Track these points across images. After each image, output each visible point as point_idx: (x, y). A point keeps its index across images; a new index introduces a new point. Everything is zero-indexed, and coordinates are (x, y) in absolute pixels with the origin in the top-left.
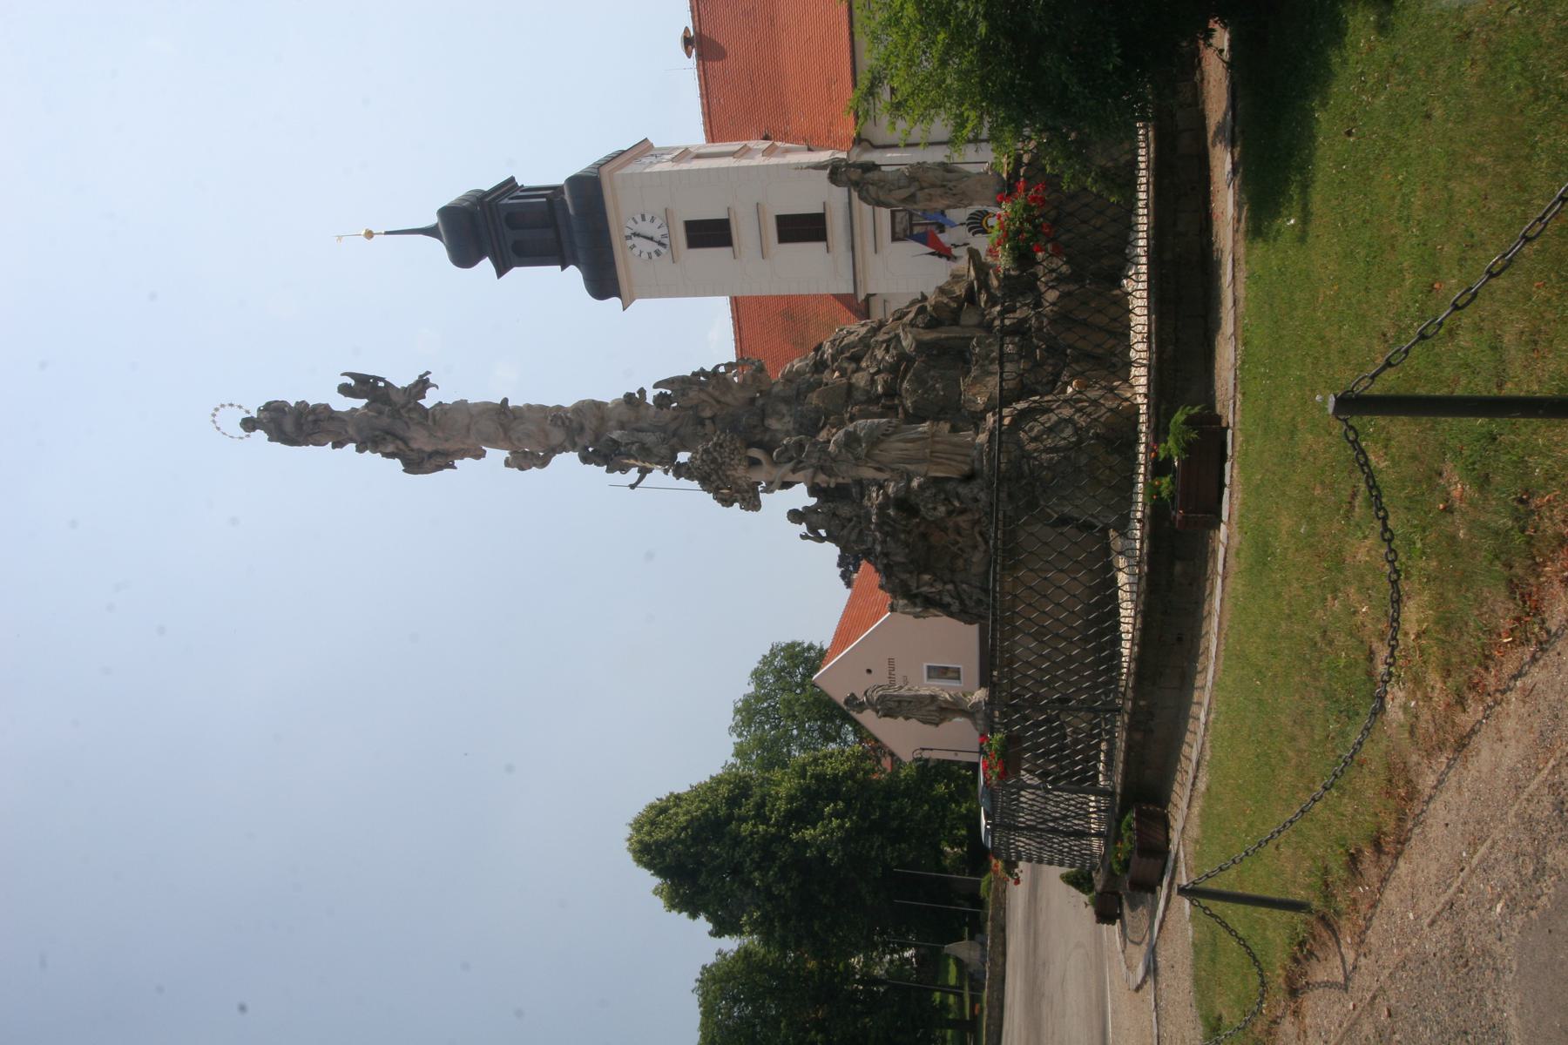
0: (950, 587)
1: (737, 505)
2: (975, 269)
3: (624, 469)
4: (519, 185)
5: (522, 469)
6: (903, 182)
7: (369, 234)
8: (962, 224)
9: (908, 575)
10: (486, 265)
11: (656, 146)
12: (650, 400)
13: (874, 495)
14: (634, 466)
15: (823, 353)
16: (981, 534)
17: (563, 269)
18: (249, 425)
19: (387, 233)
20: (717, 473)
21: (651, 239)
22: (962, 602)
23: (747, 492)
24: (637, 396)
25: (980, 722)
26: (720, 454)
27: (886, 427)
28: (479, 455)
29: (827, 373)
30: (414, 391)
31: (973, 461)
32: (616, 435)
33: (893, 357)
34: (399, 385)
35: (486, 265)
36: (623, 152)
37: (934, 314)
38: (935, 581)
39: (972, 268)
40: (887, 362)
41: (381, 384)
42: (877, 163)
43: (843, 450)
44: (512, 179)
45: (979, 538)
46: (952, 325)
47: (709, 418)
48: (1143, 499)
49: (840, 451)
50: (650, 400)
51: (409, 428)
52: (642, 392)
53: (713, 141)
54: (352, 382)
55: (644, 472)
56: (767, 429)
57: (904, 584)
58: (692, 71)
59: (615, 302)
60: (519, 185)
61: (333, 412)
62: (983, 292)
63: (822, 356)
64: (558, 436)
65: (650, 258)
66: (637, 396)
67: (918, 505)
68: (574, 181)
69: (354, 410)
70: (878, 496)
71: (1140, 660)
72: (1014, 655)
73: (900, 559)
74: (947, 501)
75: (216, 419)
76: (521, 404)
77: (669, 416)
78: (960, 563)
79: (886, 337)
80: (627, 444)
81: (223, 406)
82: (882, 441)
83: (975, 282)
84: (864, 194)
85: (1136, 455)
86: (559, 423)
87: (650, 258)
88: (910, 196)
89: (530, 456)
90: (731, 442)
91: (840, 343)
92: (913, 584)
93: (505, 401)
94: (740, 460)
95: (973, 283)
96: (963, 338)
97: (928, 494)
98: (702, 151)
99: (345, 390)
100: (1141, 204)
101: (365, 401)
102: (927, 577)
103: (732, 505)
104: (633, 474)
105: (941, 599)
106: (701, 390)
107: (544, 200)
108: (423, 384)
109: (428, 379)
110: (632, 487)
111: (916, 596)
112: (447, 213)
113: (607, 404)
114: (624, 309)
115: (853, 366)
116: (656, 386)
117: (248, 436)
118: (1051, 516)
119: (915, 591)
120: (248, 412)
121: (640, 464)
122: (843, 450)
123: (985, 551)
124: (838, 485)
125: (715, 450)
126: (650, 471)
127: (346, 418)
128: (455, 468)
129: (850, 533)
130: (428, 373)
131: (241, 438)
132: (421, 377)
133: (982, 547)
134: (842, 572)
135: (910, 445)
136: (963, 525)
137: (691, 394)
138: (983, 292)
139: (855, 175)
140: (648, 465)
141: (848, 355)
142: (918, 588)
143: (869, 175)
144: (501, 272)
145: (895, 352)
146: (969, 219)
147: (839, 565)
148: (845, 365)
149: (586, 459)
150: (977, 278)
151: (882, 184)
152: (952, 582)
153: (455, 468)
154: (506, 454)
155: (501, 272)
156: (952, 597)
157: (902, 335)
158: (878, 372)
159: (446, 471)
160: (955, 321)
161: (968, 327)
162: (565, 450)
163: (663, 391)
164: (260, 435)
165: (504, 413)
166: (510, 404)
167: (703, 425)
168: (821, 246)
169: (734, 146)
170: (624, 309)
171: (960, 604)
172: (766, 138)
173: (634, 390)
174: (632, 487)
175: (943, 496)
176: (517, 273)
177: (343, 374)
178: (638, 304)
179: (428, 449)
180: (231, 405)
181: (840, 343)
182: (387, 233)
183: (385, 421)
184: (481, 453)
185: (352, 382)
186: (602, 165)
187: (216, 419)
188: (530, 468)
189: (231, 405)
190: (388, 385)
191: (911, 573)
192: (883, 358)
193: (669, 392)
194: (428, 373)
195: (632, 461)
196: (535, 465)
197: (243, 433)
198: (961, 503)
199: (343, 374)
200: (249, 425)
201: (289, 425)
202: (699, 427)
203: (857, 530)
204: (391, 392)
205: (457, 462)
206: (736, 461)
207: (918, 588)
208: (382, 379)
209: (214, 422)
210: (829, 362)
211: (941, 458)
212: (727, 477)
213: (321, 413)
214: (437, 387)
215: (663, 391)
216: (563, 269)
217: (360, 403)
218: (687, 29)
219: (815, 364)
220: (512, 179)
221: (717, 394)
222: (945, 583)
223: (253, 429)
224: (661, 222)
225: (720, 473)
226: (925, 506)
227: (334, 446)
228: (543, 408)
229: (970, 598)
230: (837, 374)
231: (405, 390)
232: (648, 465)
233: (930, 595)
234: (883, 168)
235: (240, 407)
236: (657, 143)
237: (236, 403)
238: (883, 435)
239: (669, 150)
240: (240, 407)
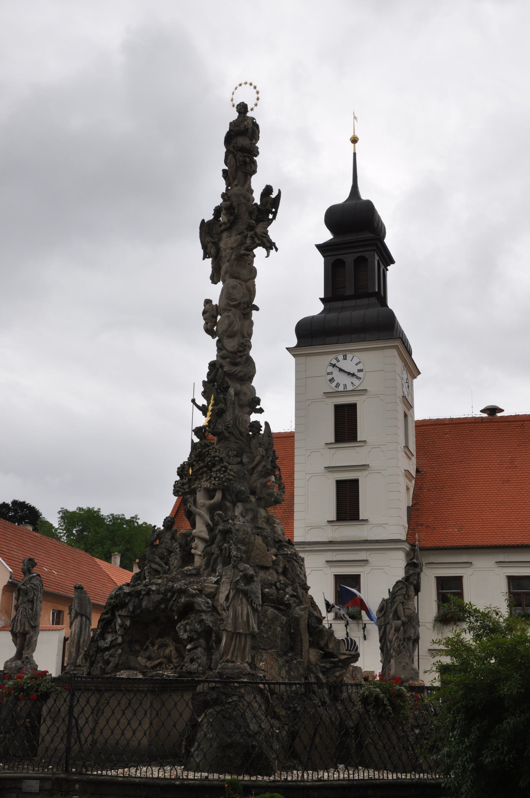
0: (120, 640)
1: (178, 478)
2: (346, 659)
3: (205, 394)
4: (388, 268)
5: (204, 313)
6: (408, 612)
7: (354, 140)
8: (347, 634)
9: (131, 610)
10: (326, 236)
11: (415, 381)
12: (254, 417)
13: (195, 587)
14: (209, 403)
15: (288, 547)
16: (160, 664)
17: (321, 299)
18: (242, 108)
19: (355, 154)
20: (205, 467)
21: (341, 370)
22: (107, 649)
23: (189, 487)
24: (258, 407)
25: (13, 665)
26: (219, 470)
27: (257, 603)
28: (214, 279)
29: (274, 550)
30: (265, 240)
31: (233, 662)
32: (232, 391)
33: (288, 600)
34: (269, 229)
35: (326, 236)
36: (410, 353)
37: (318, 630)
38: (125, 629)
39: (346, 656)
40: (285, 596)
41: (271, 216)
42: (419, 593)
43: (241, 574)
44: (392, 262)
45: (156, 662)
46: (310, 641)
47: (242, 460)
48: (228, 780)
49: (241, 571)
50: (254, 417)
51: (239, 234)
52: (261, 411)
53: (416, 426)
54: (273, 196)
55: (204, 410)
56: (234, 504)
57: (124, 605)
58: (470, 413)
59: (293, 342)
60: (388, 268)
61: (251, 176)
62: (331, 665)
63: (285, 546)
64: (231, 344)
65: (328, 374)
66: (258, 407)
67: (189, 618)
68: (391, 317)
69: (252, 191)
70: (194, 589)
71: (112, 783)
72: (103, 693)
73: (144, 604)
74: (190, 640)
75: (248, 85)
76: (253, 318)
77: (243, 430)
78: (138, 648)
79: (301, 595)
80: (225, 399)
81: (258, 93)
82: (248, 600)
83: (337, 659)
84: (401, 586)
85: (256, 774)
86: (241, 349)
87: (328, 374)
88: (398, 616)
89: (213, 320)
90: (228, 479)
91: (295, 560)
92: (123, 612)
93: (257, 309)
94: (214, 484)
95: (337, 657)
96: (301, 651)
97: (198, 626)
98: (409, 418)
99: (268, 190)
100: (399, 775)
101: (259, 203)
102: (128, 623)
103: (178, 474)
104: (202, 401)
105: (109, 633)
106: (263, 456)
107: (377, 290)
108: (270, 246)
109: (272, 249)
110: (193, 401)
111: (113, 615)
112: (369, 206)
113: (251, 383)
114: (287, 348)
115: (280, 570)
116: (267, 424)
117: (233, 106)
118: (199, 716)
119: (117, 614)
120: (252, 110)
121: (210, 408)
122: (241, 574)
123: (146, 667)
124: (193, 555)
125: (222, 467)
126: (205, 414)
127: (246, 187)
128: (204, 259)
129: (157, 563)
130: (277, 250)
131: (232, 100)
132: (274, 244)
133: (149, 664)
134: (8, 505)
135: (245, 618)
136: (167, 651)
137: (261, 449)
138: (331, 665)
139: (413, 580)
140: (209, 414)
141: (287, 566)
142: (120, 616)
143: (412, 588)
144: (322, 248)
145: (291, 602)
146: (351, 639)
147: (15, 503)
148: (281, 565)
149: (212, 365)
150: (340, 661)
151: (407, 597)
152: (123, 642)
153: (204, 259)
154: (216, 301)
155: (322, 248)
156: (112, 641)
157: (302, 607)
158: (278, 589)
159: (201, 252)
160: (312, 644)
161: (309, 653)
162: (219, 349)
163: (263, 429)
164: (234, 115)
165: (248, 307)
166: (254, 312)
167: (237, 456)
168: (333, 517)
169: (413, 447)
170: (287, 348)
171: (106, 647)
172: (418, 471)
173: (262, 405)
174: (193, 401)
175: (195, 637)
176: (319, 261)
177: (279, 191)
178: (291, 360)
179: (222, 245)
180: (258, 99)
181: (295, 560)
182: (355, 154)
183: (245, 217)
184: (215, 279)
185: (273, 196)
186: (402, 339)
187: (248, 85)
188: (205, 319)
189: (258, 99)
190: (270, 222)
191: (133, 611)
192: (287, 593)
193: (262, 432)
194: (277, 250)
195: (212, 402)
196: (206, 323)
197: (237, 102)
198: (189, 650)
199: (279, 191)
200: (242, 108)
201: (242, 141)
202: (235, 453)
203: (159, 568)
204: (266, 223)
205: (209, 261)
206: (213, 482)
207: (120, 616)
208: (274, 218)
209: (246, 83)
210: (281, 552)
211: (236, 641)
212: (202, 474)
213: (251, 167)
214: (267, 257)
215: (263, 429)
216: (321, 299)
217: (257, 200)
218: (502, 411)
219: (280, 541)
220: (392, 262)
221: (260, 468)
222: (122, 636)
223: (239, 111)
224: (357, 385)
225: (205, 469)
226: (187, 624)
227: (224, 171)
228: (250, 335)
229: (111, 656)
230: (274, 558)
231: (266, 233)
232: (209, 414)
233: (113, 624)
234: (416, 597)
235: (256, 105)
236: (416, 382)
237: (259, 95)
238: (252, 601)
239: (411, 394)
240: (256, 105)
